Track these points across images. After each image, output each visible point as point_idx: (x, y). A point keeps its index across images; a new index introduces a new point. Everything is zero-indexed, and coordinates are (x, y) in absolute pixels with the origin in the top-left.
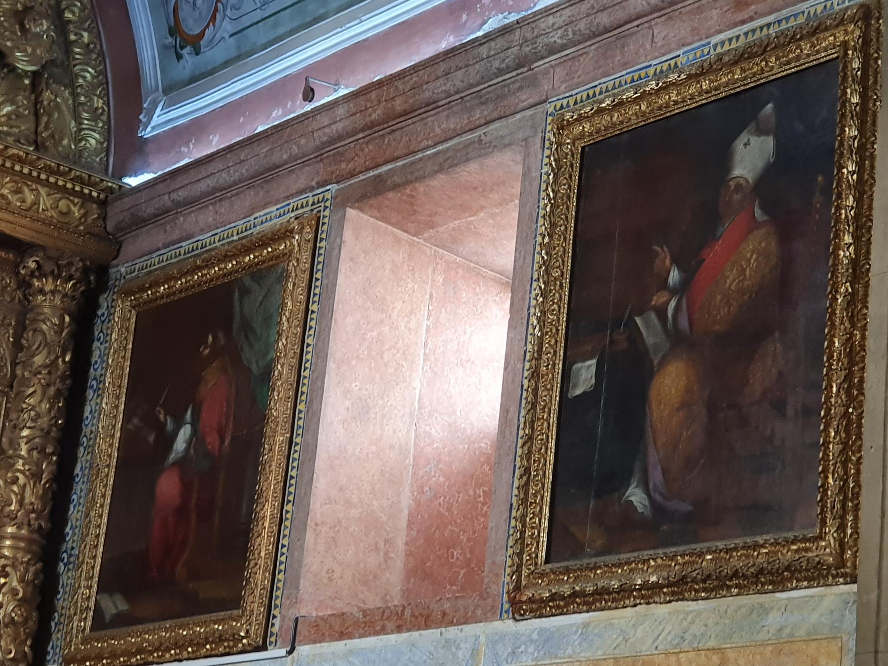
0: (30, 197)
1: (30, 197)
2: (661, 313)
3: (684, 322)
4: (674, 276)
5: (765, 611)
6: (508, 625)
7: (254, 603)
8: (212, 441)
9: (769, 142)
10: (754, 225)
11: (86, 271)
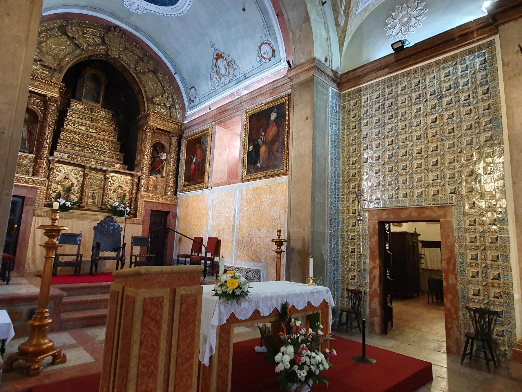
0: (170, 125)
1: (170, 125)
2: (261, 139)
3: (264, 140)
4: (263, 134)
5: (276, 179)
6: (241, 183)
7: (206, 182)
8: (199, 159)
9: (276, 114)
10: (274, 126)
11: (179, 136)
